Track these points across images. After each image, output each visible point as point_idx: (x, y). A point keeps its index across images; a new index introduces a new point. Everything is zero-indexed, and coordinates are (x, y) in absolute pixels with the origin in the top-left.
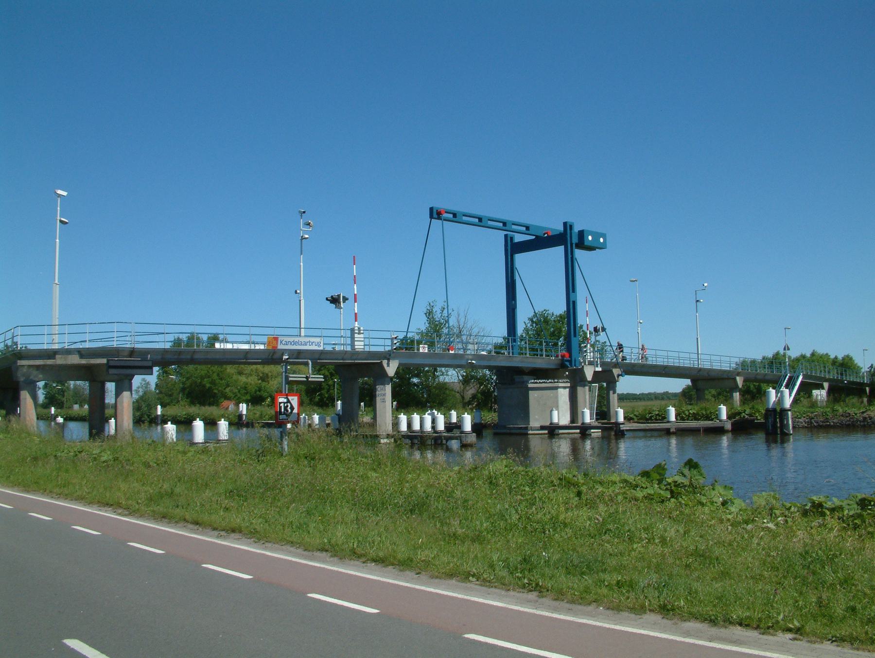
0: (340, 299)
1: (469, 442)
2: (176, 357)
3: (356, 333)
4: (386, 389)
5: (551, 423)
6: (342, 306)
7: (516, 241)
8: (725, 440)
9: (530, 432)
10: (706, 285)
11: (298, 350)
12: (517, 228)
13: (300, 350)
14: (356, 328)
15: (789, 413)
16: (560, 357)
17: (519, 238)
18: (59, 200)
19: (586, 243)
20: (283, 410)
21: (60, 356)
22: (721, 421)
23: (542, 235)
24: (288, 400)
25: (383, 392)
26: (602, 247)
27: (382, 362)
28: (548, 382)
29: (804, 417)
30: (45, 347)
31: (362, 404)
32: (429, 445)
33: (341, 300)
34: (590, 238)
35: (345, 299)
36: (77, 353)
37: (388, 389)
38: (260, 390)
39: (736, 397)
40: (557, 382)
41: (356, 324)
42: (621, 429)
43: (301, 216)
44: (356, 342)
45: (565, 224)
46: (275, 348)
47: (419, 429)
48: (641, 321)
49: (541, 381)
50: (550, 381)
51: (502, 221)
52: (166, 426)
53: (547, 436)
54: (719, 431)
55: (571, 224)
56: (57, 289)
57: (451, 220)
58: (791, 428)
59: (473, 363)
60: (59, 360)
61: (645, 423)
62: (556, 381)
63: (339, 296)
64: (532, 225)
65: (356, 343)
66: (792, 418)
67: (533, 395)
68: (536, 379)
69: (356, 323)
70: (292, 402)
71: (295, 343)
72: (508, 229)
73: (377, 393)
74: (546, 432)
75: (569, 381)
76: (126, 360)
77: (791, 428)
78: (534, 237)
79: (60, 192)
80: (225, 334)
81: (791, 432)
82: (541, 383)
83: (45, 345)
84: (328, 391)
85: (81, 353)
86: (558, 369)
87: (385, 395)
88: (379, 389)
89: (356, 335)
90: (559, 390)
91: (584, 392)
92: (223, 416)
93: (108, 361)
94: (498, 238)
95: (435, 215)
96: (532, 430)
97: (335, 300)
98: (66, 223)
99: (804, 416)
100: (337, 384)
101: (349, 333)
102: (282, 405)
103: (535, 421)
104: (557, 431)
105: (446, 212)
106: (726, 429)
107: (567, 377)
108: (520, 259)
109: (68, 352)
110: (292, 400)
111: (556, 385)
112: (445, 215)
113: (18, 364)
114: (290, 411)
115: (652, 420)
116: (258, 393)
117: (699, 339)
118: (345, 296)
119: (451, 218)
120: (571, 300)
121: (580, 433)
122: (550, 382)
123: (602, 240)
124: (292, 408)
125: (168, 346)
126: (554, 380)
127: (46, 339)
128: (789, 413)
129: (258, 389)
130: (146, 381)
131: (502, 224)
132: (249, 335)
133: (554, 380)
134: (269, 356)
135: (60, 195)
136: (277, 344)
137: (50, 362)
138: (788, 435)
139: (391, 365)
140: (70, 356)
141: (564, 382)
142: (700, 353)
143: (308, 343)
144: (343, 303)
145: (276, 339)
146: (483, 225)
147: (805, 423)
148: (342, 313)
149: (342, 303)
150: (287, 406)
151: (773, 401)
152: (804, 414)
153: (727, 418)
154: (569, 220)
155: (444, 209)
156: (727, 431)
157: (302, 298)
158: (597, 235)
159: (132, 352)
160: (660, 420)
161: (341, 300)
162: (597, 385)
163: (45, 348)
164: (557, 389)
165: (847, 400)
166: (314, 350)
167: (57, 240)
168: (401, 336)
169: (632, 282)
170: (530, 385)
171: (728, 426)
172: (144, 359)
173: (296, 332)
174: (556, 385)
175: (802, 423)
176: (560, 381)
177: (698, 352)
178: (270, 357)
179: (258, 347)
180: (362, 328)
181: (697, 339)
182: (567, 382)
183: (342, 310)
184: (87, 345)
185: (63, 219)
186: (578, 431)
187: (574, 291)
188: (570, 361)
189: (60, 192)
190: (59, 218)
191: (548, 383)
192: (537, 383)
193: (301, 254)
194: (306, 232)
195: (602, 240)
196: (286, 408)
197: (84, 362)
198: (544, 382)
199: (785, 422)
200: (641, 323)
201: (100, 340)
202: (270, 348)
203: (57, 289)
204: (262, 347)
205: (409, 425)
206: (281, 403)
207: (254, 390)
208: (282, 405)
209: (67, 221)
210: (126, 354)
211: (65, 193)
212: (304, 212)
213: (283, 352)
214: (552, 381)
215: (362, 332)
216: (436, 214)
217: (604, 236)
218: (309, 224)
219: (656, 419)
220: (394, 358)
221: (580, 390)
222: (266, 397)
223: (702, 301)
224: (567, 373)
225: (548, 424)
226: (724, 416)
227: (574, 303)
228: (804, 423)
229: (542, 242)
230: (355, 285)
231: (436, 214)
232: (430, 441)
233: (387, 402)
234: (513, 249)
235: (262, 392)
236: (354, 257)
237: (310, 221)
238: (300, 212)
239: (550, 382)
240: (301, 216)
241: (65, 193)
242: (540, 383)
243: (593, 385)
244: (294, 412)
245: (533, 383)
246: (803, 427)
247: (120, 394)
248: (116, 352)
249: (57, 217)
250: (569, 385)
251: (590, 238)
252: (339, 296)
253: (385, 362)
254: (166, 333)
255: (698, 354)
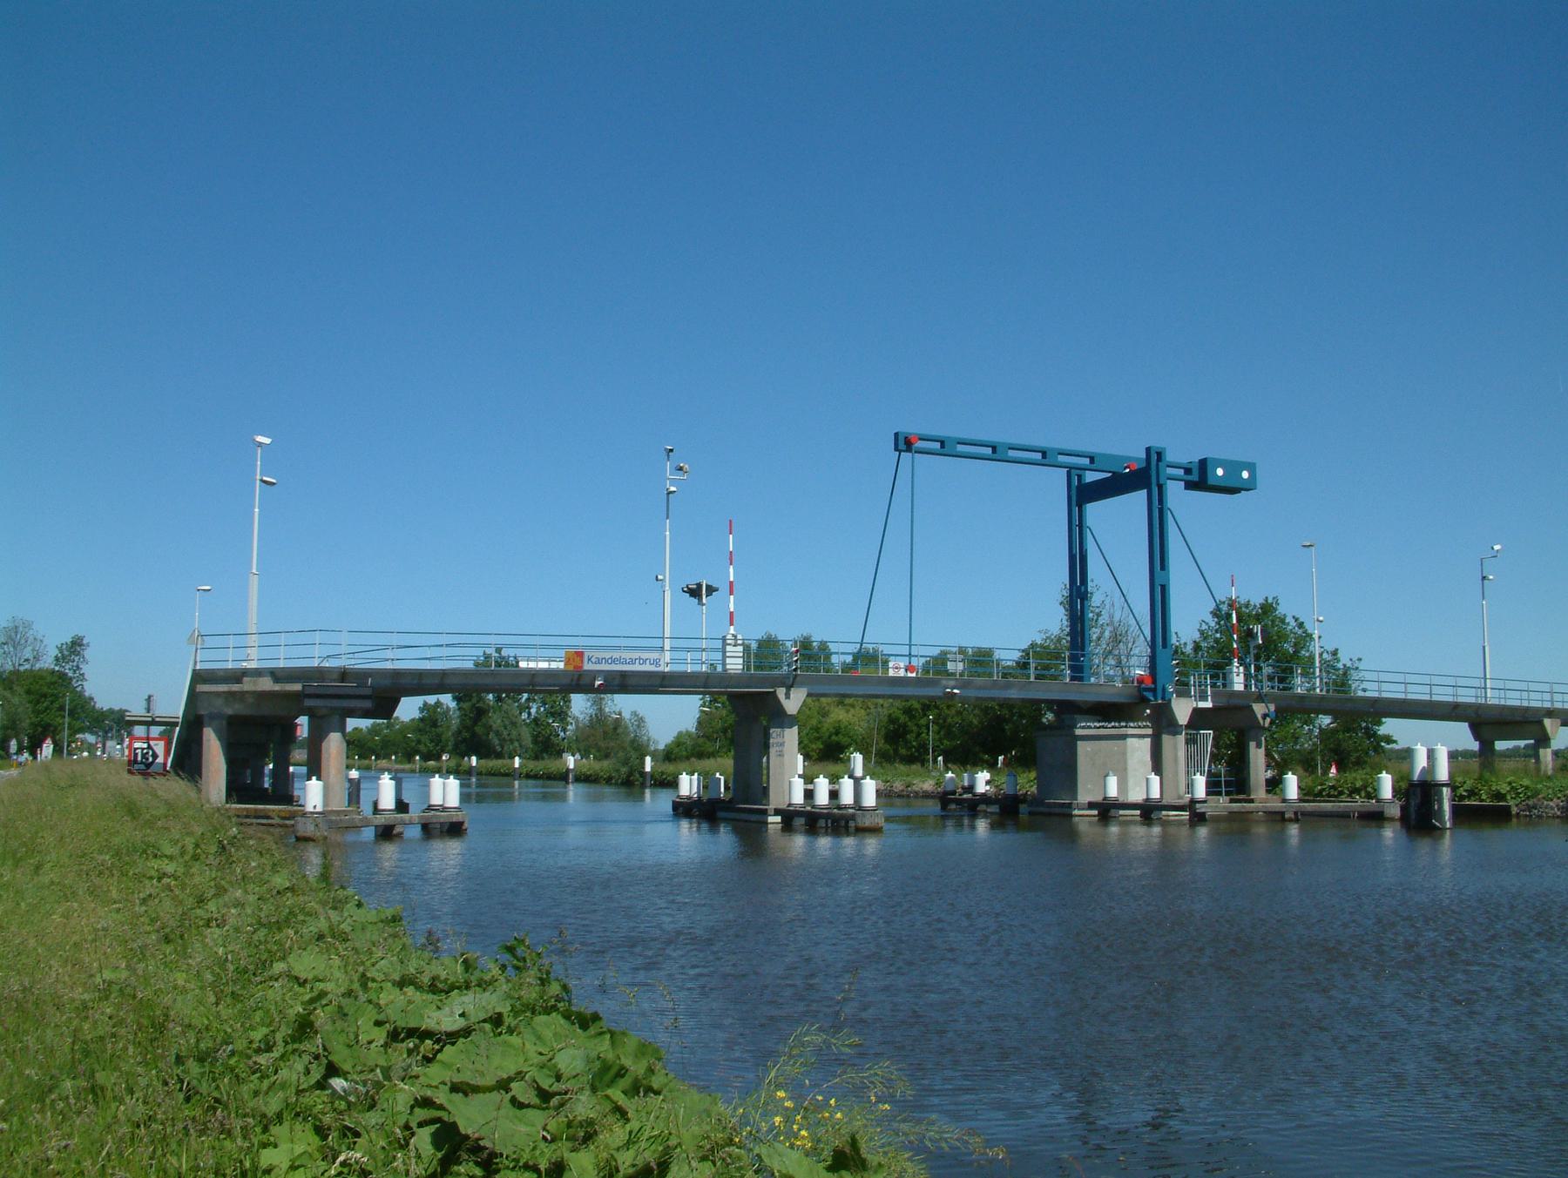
0: (702, 591)
1: (867, 825)
2: (415, 682)
3: (730, 644)
4: (785, 735)
5: (1105, 798)
6: (704, 601)
7: (1087, 481)
8: (1389, 833)
9: (1076, 812)
10: (1497, 547)
11: (622, 671)
12: (1027, 456)
13: (625, 671)
14: (729, 637)
15: (1445, 789)
16: (1135, 684)
17: (1090, 477)
18: (259, 451)
19: (1211, 481)
20: (139, 759)
21: (248, 679)
22: (1379, 801)
23: (1120, 471)
24: (149, 745)
25: (780, 740)
26: (1249, 487)
27: (775, 691)
28: (1109, 726)
29: (1559, 798)
30: (230, 666)
31: (940, 758)
32: (822, 827)
33: (704, 592)
34: (1220, 472)
35: (711, 590)
36: (269, 674)
37: (791, 736)
38: (837, 734)
39: (1545, 756)
40: (1126, 727)
41: (732, 630)
42: (1198, 811)
43: (668, 456)
44: (727, 659)
45: (1148, 450)
46: (579, 668)
47: (1158, 796)
48: (1321, 618)
49: (1098, 725)
50: (1113, 724)
51: (1040, 449)
52: (431, 780)
53: (1097, 818)
54: (1376, 818)
55: (1160, 450)
56: (254, 582)
57: (990, 457)
58: (1447, 818)
59: (956, 694)
60: (248, 685)
61: (1314, 801)
62: (1123, 724)
63: (699, 586)
64: (1100, 454)
65: (728, 661)
66: (498, 793)
67: (1083, 748)
68: (1102, 722)
69: (732, 627)
70: (155, 748)
71: (614, 661)
72: (1099, 468)
73: (771, 741)
74: (1096, 812)
75: (1148, 724)
76: (332, 686)
77: (1447, 818)
78: (1110, 474)
79: (260, 439)
80: (842, 653)
81: (1448, 825)
82: (1099, 728)
83: (282, 661)
84: (919, 734)
85: (277, 675)
86: (1137, 703)
87: (787, 741)
88: (774, 735)
89: (729, 648)
90: (1129, 740)
91: (1175, 748)
92: (1549, 778)
93: (304, 686)
94: (1055, 484)
95: (902, 446)
96: (1079, 809)
97: (695, 592)
98: (274, 484)
99: (1559, 795)
100: (933, 723)
101: (719, 644)
102: (139, 751)
103: (1086, 794)
104: (1113, 812)
105: (920, 439)
106: (1388, 816)
107: (1149, 718)
108: (1096, 512)
109: (258, 673)
110: (156, 745)
111: (1123, 731)
112: (919, 444)
113: (198, 690)
114: (151, 759)
115: (1323, 796)
116: (834, 737)
117: (1487, 649)
118: (710, 584)
119: (937, 449)
120: (1158, 582)
121: (1098, 816)
122: (1113, 727)
123: (1245, 475)
124: (155, 756)
125: (469, 665)
126: (1127, 722)
127: (231, 654)
128: (1445, 789)
129: (834, 731)
130: (638, 716)
131: (1088, 460)
132: (862, 641)
133: (1119, 722)
134: (572, 680)
135: (260, 444)
136: (582, 661)
137: (235, 687)
138: (1443, 829)
139: (792, 696)
140: (261, 679)
141: (1140, 727)
142: (1488, 676)
143: (637, 661)
144: (707, 596)
145: (580, 654)
146: (999, 458)
147: (1558, 810)
148: (704, 612)
149: (704, 597)
150: (147, 753)
151: (1420, 768)
152: (1560, 791)
153: (1394, 796)
154: (1156, 443)
155: (916, 434)
156: (1392, 819)
157: (667, 588)
158: (1233, 467)
159: (344, 674)
160: (1335, 796)
161: (704, 592)
162: (1211, 732)
163: (230, 667)
164: (1125, 739)
165: (884, 764)
166: (649, 672)
167: (257, 510)
168: (854, 648)
169: (1306, 549)
170: (1078, 732)
171: (1394, 811)
172: (362, 685)
173: (658, 643)
174: (1123, 731)
175: (1552, 808)
176: (1132, 725)
177: (1485, 676)
178: (574, 683)
179: (554, 665)
180: (739, 637)
181: (1484, 647)
182: (1147, 727)
183: (704, 607)
184: (282, 664)
185: (265, 478)
186: (1138, 812)
187: (1163, 566)
188: (1154, 691)
189: (260, 439)
190: (258, 477)
191: (1110, 729)
192: (1090, 727)
193: (667, 518)
194: (673, 482)
195: (1245, 475)
196: (144, 756)
197: (277, 687)
198: (1103, 727)
199: (1436, 807)
200: (1321, 621)
201: (465, 658)
202: (571, 668)
203: (254, 582)
204: (561, 665)
205: (834, 795)
206: (138, 748)
207: (827, 734)
208: (139, 751)
209: (274, 481)
210: (335, 676)
211: (267, 441)
212: (671, 450)
213: (594, 674)
214: (1117, 724)
215: (740, 642)
216: (905, 444)
217: (1251, 467)
218: (681, 469)
219: (1329, 795)
220: (802, 685)
221: (1166, 739)
222: (847, 743)
223: (1491, 577)
224: (1148, 711)
225: (1098, 798)
226: (1387, 791)
227: (1164, 588)
228: (1556, 809)
229: (1117, 484)
230: (731, 567)
231: (905, 444)
232: (824, 820)
233: (785, 756)
234: (1083, 494)
235: (840, 736)
236: (730, 521)
237: (682, 465)
238: (666, 449)
239: (1113, 727)
240: (668, 456)
241: (267, 441)
242: (1095, 727)
243: (1202, 732)
244: (157, 761)
245: (1083, 727)
246: (1555, 817)
247: (325, 738)
248: (319, 673)
249: (256, 475)
250: (1150, 731)
251: (1220, 472)
252: (699, 586)
253: (781, 692)
254: (442, 645)
255: (1485, 679)
